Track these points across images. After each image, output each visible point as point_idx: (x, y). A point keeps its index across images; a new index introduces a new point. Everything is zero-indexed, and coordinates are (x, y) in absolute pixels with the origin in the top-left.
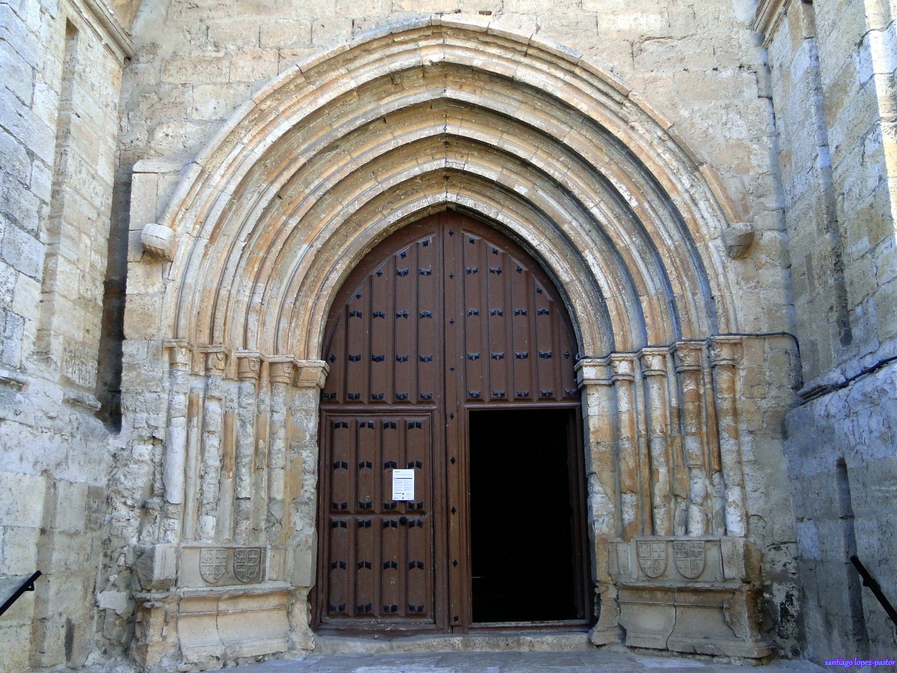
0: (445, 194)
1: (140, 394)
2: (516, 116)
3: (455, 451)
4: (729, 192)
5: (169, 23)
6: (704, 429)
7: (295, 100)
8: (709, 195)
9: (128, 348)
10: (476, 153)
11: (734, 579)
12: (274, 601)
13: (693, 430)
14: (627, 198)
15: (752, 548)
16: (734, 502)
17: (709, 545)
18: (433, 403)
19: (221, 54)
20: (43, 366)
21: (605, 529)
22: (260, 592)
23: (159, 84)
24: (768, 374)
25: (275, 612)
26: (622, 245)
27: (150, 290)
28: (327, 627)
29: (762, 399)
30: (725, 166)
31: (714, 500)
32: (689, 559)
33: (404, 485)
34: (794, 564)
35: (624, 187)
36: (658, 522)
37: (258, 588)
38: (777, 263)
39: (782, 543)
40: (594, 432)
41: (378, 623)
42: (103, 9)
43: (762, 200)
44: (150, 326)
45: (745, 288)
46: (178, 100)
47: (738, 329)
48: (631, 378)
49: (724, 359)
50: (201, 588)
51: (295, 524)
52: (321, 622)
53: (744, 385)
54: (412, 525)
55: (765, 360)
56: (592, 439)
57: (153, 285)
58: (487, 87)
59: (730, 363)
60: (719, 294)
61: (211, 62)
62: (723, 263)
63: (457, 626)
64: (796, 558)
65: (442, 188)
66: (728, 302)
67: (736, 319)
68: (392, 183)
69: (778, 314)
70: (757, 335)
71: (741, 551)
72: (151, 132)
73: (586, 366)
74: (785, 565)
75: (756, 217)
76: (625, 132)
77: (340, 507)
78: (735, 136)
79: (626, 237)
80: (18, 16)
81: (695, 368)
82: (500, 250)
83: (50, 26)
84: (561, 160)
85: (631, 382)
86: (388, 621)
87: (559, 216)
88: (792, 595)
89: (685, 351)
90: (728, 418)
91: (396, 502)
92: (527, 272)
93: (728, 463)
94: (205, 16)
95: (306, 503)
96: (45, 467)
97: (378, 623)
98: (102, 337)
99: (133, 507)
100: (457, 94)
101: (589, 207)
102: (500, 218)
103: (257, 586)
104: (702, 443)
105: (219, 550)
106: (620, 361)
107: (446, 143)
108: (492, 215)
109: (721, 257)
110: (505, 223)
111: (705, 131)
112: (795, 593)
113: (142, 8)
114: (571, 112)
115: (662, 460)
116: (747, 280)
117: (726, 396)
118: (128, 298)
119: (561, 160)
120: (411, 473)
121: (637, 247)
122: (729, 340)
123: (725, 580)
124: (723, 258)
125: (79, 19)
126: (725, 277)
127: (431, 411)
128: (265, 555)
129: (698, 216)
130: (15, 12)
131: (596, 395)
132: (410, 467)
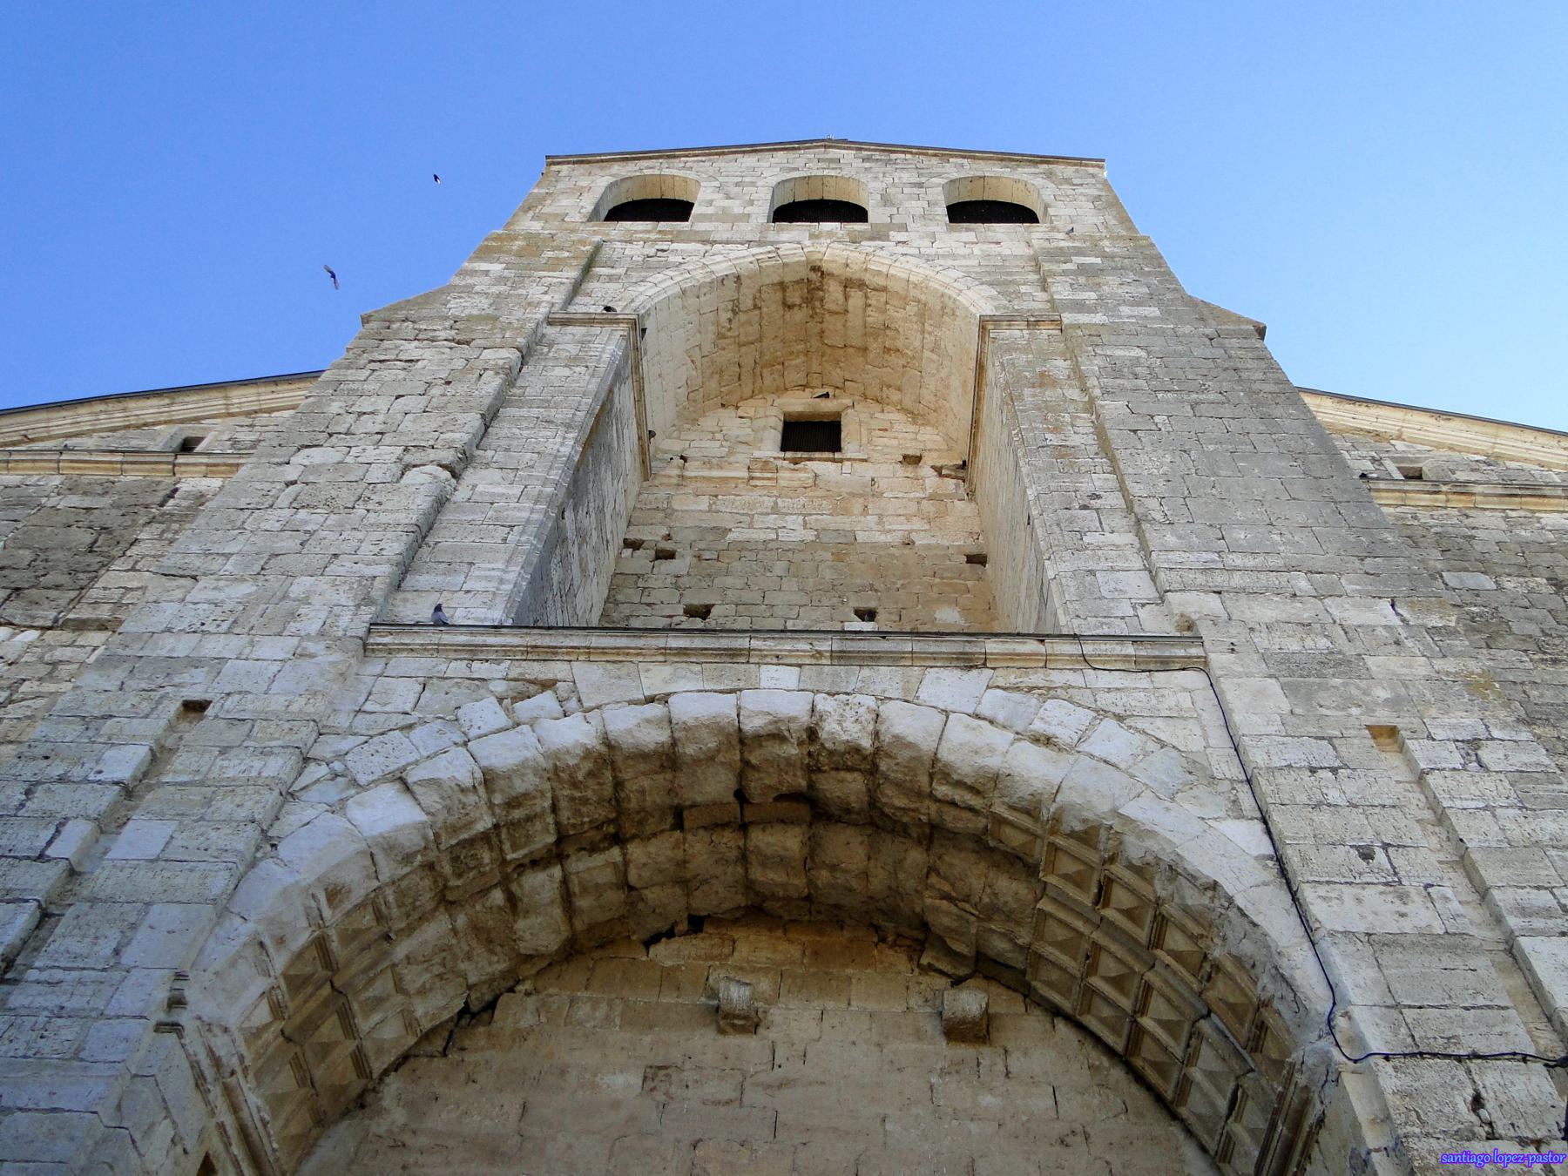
4: (245, 1114)
5: (354, 1167)
20: (1484, 1094)
42: (265, 1140)
80: (136, 1147)
83: (176, 1163)
94: (412, 1160)
96: (1058, 1148)
113: (322, 1142)
125: (224, 1155)
130: (133, 1142)
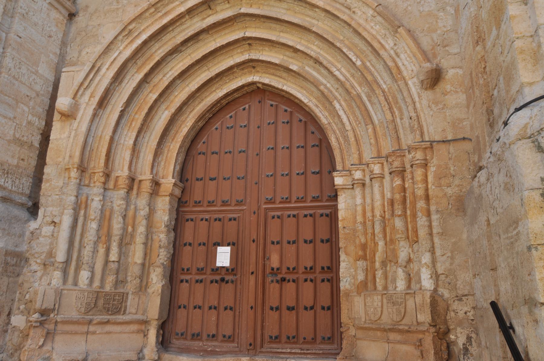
0: (252, 77)
1: (50, 196)
2: (283, 18)
3: (255, 235)
6: (408, 212)
7: (150, 23)
8: (406, 48)
9: (46, 170)
10: (267, 49)
11: (424, 323)
12: (134, 327)
13: (400, 213)
14: (354, 60)
15: (439, 299)
16: (426, 263)
17: (408, 297)
18: (244, 205)
19: (120, 6)
21: (348, 286)
22: (120, 321)
23: (87, 26)
24: (452, 169)
25: (135, 334)
26: (355, 93)
27: (62, 137)
28: (174, 346)
29: (448, 187)
30: (420, 29)
31: (415, 263)
32: (395, 307)
33: (223, 257)
34: (472, 312)
35: (352, 54)
36: (378, 280)
37: (120, 318)
38: (459, 90)
39: (463, 296)
40: (344, 220)
41: (204, 345)
43: (447, 48)
44: (59, 157)
45: (435, 110)
46: (95, 33)
47: (430, 138)
48: (363, 182)
49: (417, 160)
50: (74, 315)
51: (152, 279)
52: (170, 342)
53: (434, 177)
54: (227, 282)
55: (450, 159)
56: (340, 225)
57: (64, 133)
58: (266, 4)
59: (423, 162)
60: (415, 115)
61: (114, 11)
62: (418, 93)
63: (251, 349)
64: (474, 308)
65: (252, 74)
66: (423, 120)
67: (428, 131)
68: (217, 71)
69: (461, 125)
70: (443, 141)
71: (429, 301)
72: (80, 52)
73: (336, 176)
74: (466, 313)
75: (442, 60)
76: (349, 15)
77: (185, 270)
78: (427, 9)
79: (359, 88)
81: (401, 169)
82: (289, 110)
84: (316, 44)
85: (364, 185)
86: (210, 344)
87: (318, 80)
88: (471, 337)
89: (393, 158)
90: (421, 201)
91: (218, 267)
92: (305, 122)
93: (422, 235)
95: (159, 267)
97: (204, 345)
98: (37, 164)
99: (40, 264)
100: (248, 10)
101: (333, 71)
102: (285, 88)
103: (121, 317)
104: (406, 222)
105: (89, 292)
106: (356, 170)
107: (249, 44)
108: (280, 87)
109: (417, 89)
110: (288, 90)
111: (405, 9)
112: (473, 335)
114: (317, 10)
115: (381, 236)
116: (436, 103)
117: (420, 186)
118: (50, 142)
119: (316, 44)
120: (228, 249)
121: (365, 93)
122: (422, 145)
123: (418, 324)
124: (419, 90)
126: (420, 103)
127: (243, 210)
128: (127, 298)
129: (400, 64)
131: (344, 195)
132: (228, 245)
